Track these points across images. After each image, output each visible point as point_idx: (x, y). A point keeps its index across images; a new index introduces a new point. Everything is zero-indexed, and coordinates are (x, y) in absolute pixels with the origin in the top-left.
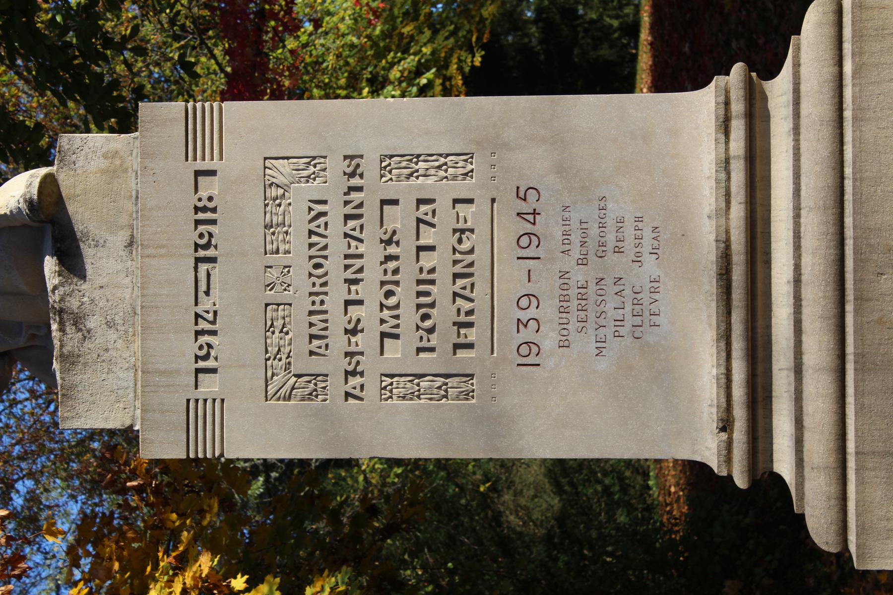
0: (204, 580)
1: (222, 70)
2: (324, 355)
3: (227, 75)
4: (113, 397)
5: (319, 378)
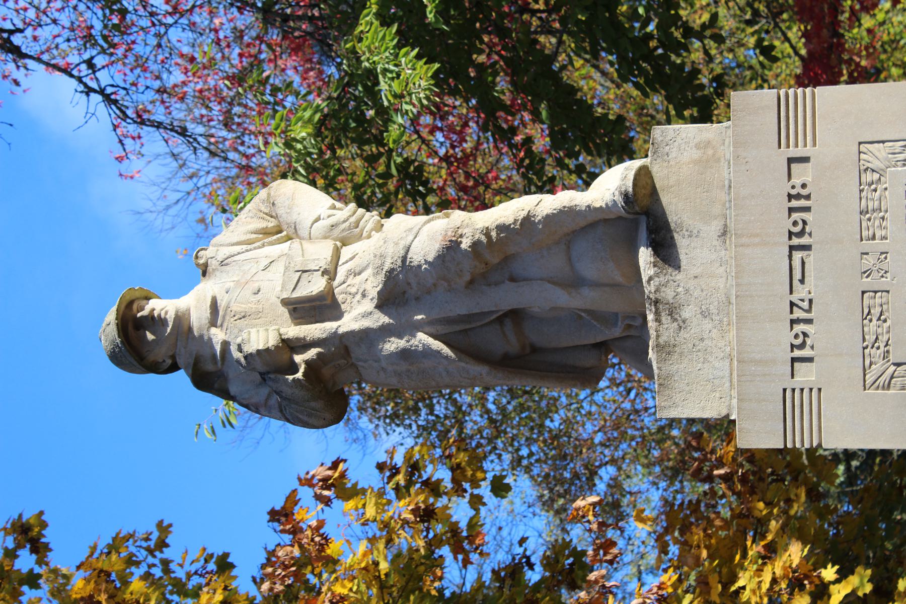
0: (794, 572)
1: (797, 53)
3: (801, 58)
4: (709, 387)
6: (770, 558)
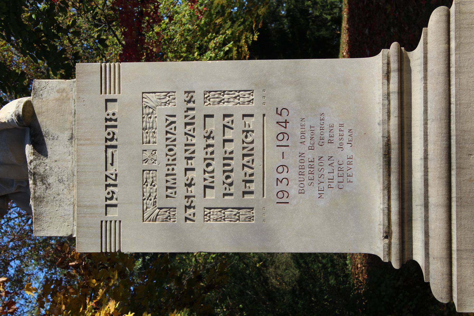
1: (120, 43)
2: (174, 198)
3: (123, 45)
4: (62, 220)
5: (171, 210)
6: (98, 309)
